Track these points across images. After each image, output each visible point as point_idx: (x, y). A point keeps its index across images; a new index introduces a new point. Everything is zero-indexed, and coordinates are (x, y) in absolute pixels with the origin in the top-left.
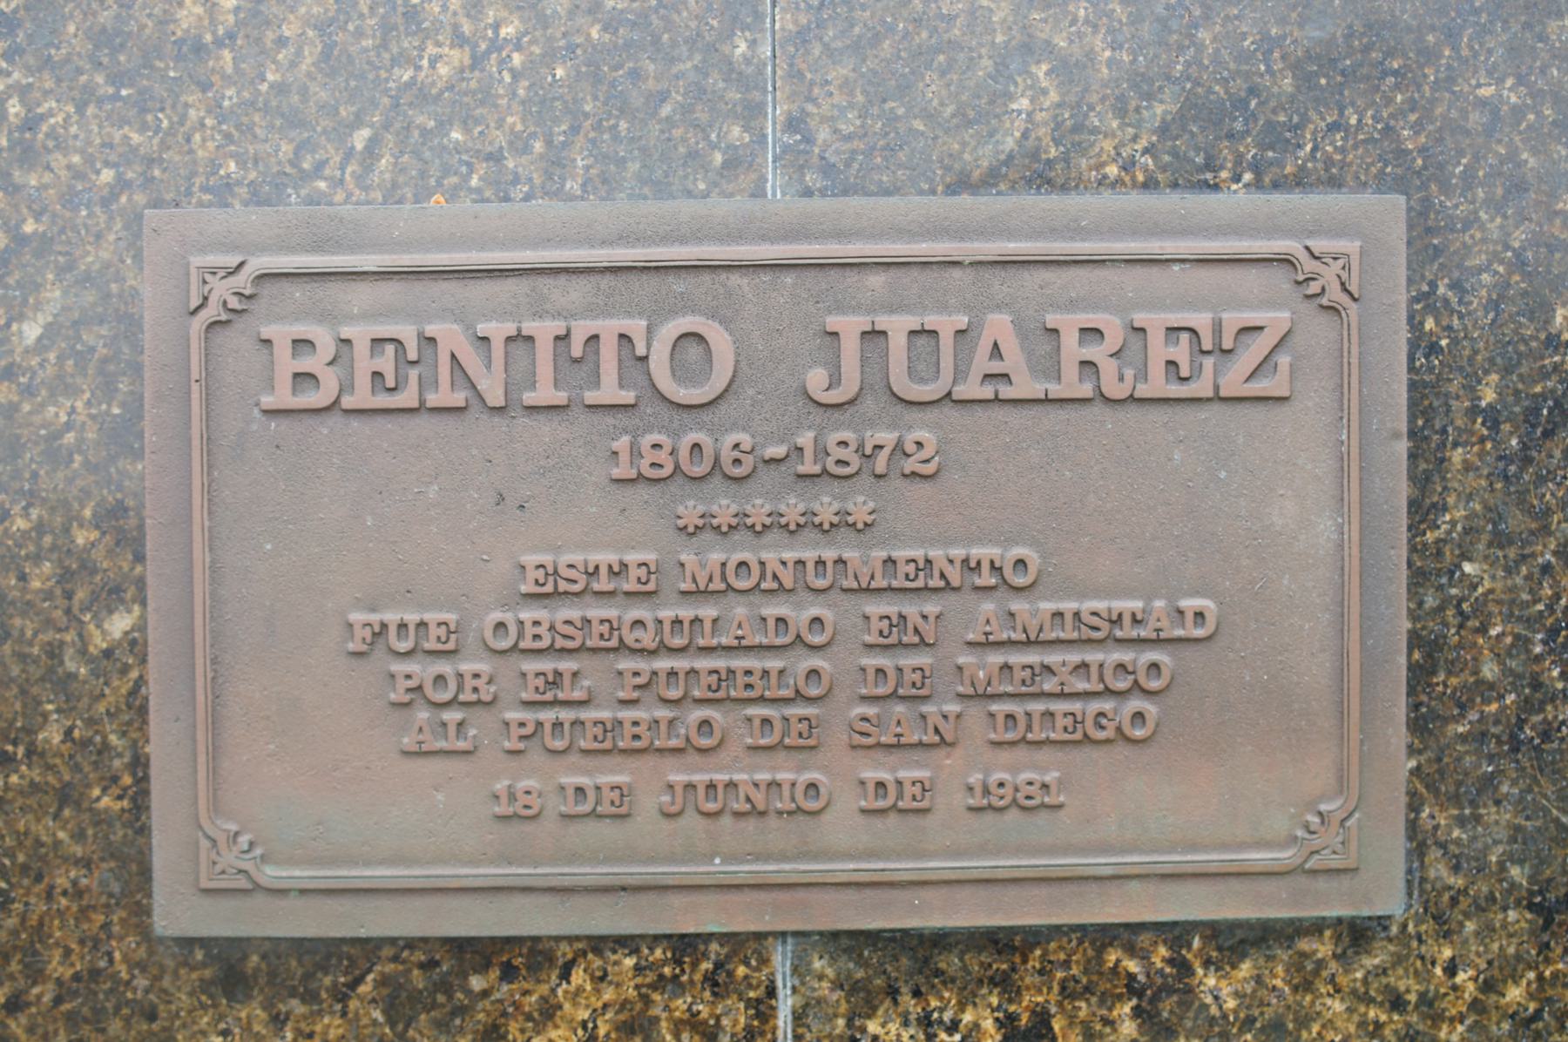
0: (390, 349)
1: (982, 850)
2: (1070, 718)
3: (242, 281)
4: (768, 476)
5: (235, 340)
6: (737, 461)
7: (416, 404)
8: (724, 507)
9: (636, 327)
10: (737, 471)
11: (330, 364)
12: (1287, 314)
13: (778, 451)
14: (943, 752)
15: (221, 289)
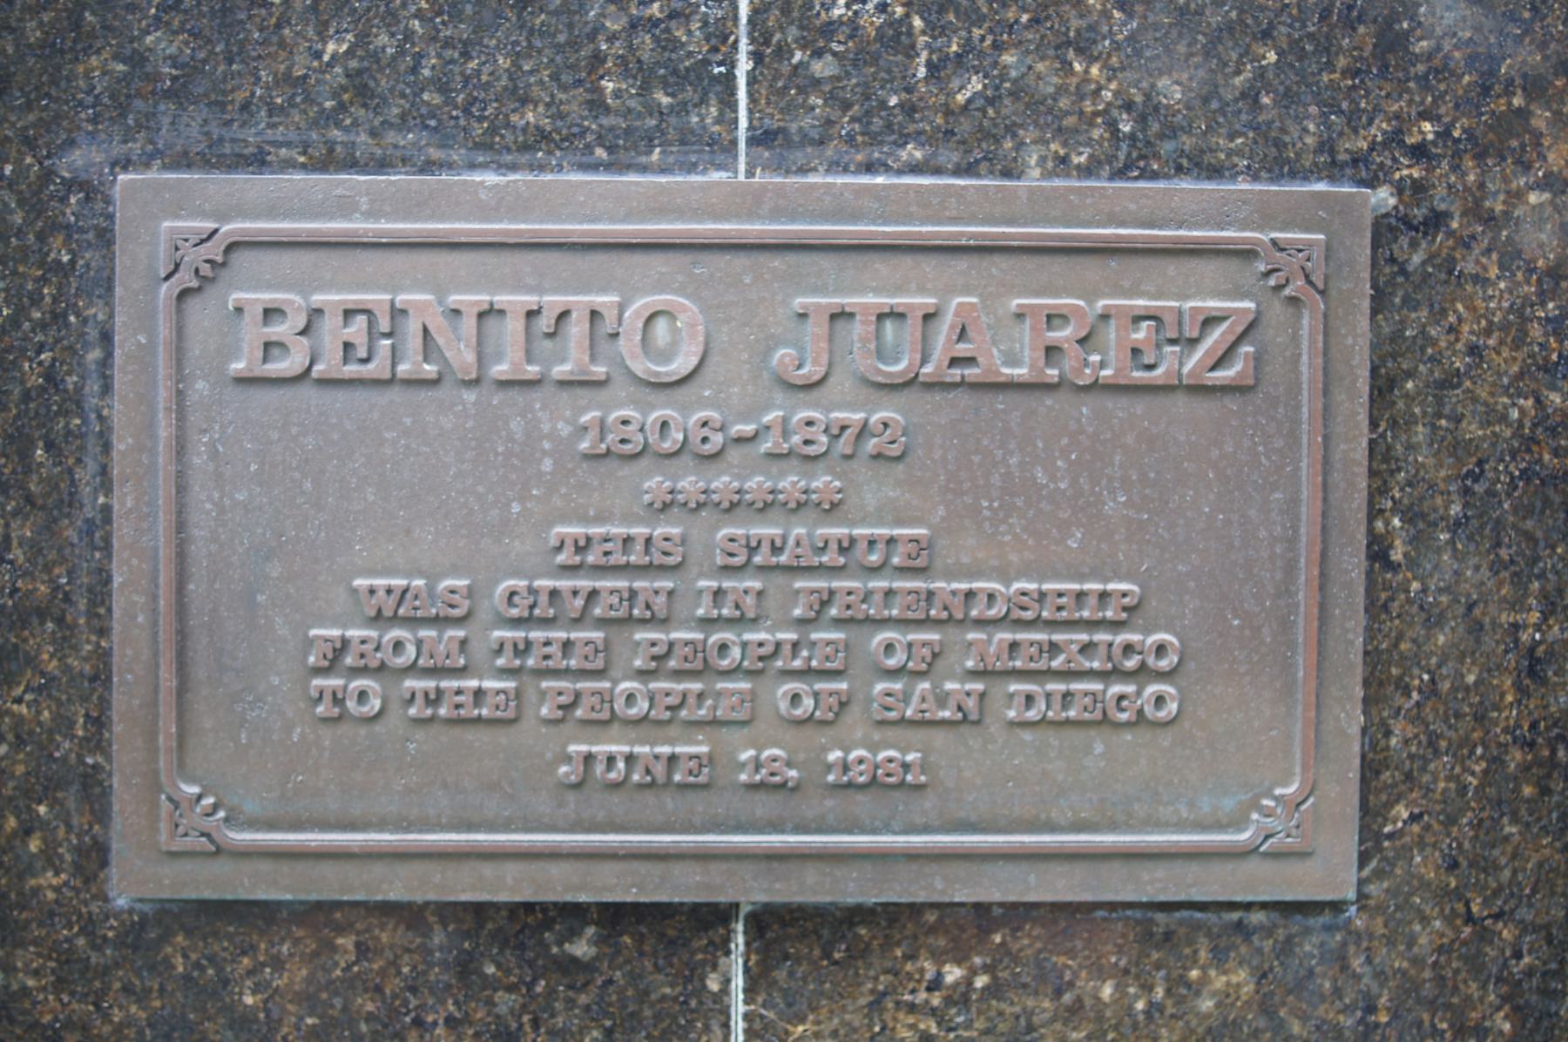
0: (361, 320)
1: (776, 827)
2: (503, 697)
3: (214, 250)
4: (734, 455)
5: (201, 313)
6: (705, 440)
7: (387, 375)
8: (689, 484)
9: (605, 300)
10: (708, 448)
11: (301, 333)
12: (1252, 305)
13: (748, 428)
14: (964, 729)
15: (194, 256)
